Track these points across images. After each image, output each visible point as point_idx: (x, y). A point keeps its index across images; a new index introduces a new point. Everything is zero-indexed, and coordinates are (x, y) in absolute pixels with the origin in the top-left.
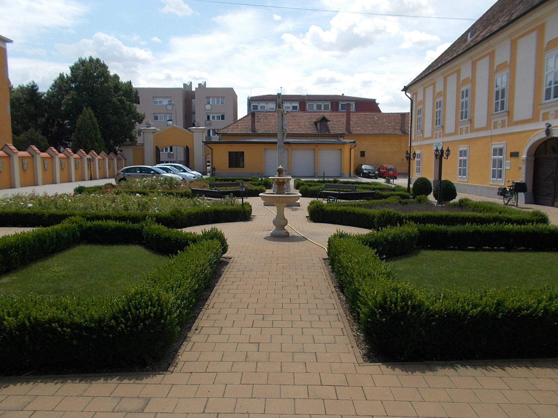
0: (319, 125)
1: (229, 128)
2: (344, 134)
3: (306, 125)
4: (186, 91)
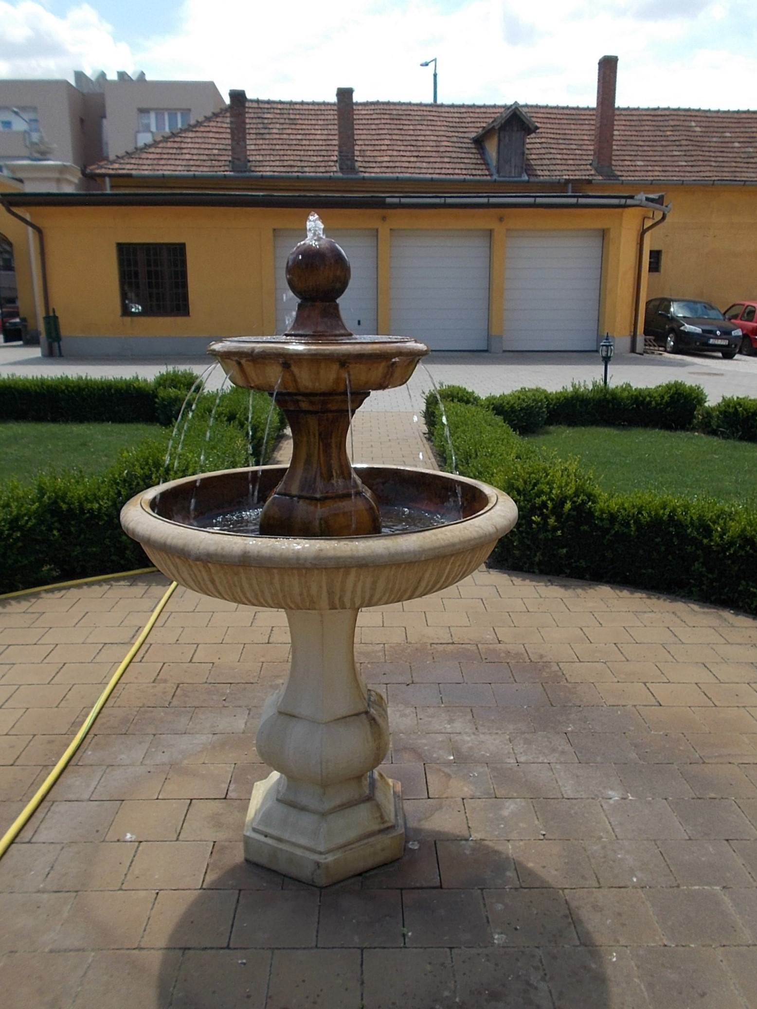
0: (492, 148)
1: (144, 156)
2: (589, 182)
3: (442, 149)
4: (83, 95)
